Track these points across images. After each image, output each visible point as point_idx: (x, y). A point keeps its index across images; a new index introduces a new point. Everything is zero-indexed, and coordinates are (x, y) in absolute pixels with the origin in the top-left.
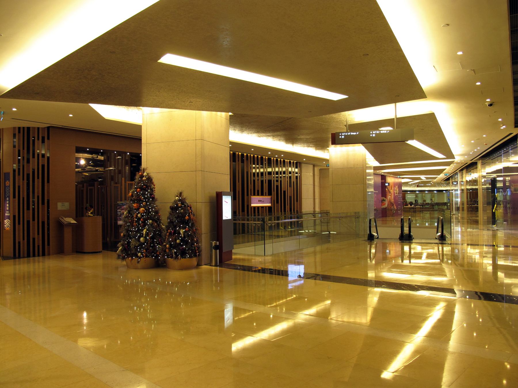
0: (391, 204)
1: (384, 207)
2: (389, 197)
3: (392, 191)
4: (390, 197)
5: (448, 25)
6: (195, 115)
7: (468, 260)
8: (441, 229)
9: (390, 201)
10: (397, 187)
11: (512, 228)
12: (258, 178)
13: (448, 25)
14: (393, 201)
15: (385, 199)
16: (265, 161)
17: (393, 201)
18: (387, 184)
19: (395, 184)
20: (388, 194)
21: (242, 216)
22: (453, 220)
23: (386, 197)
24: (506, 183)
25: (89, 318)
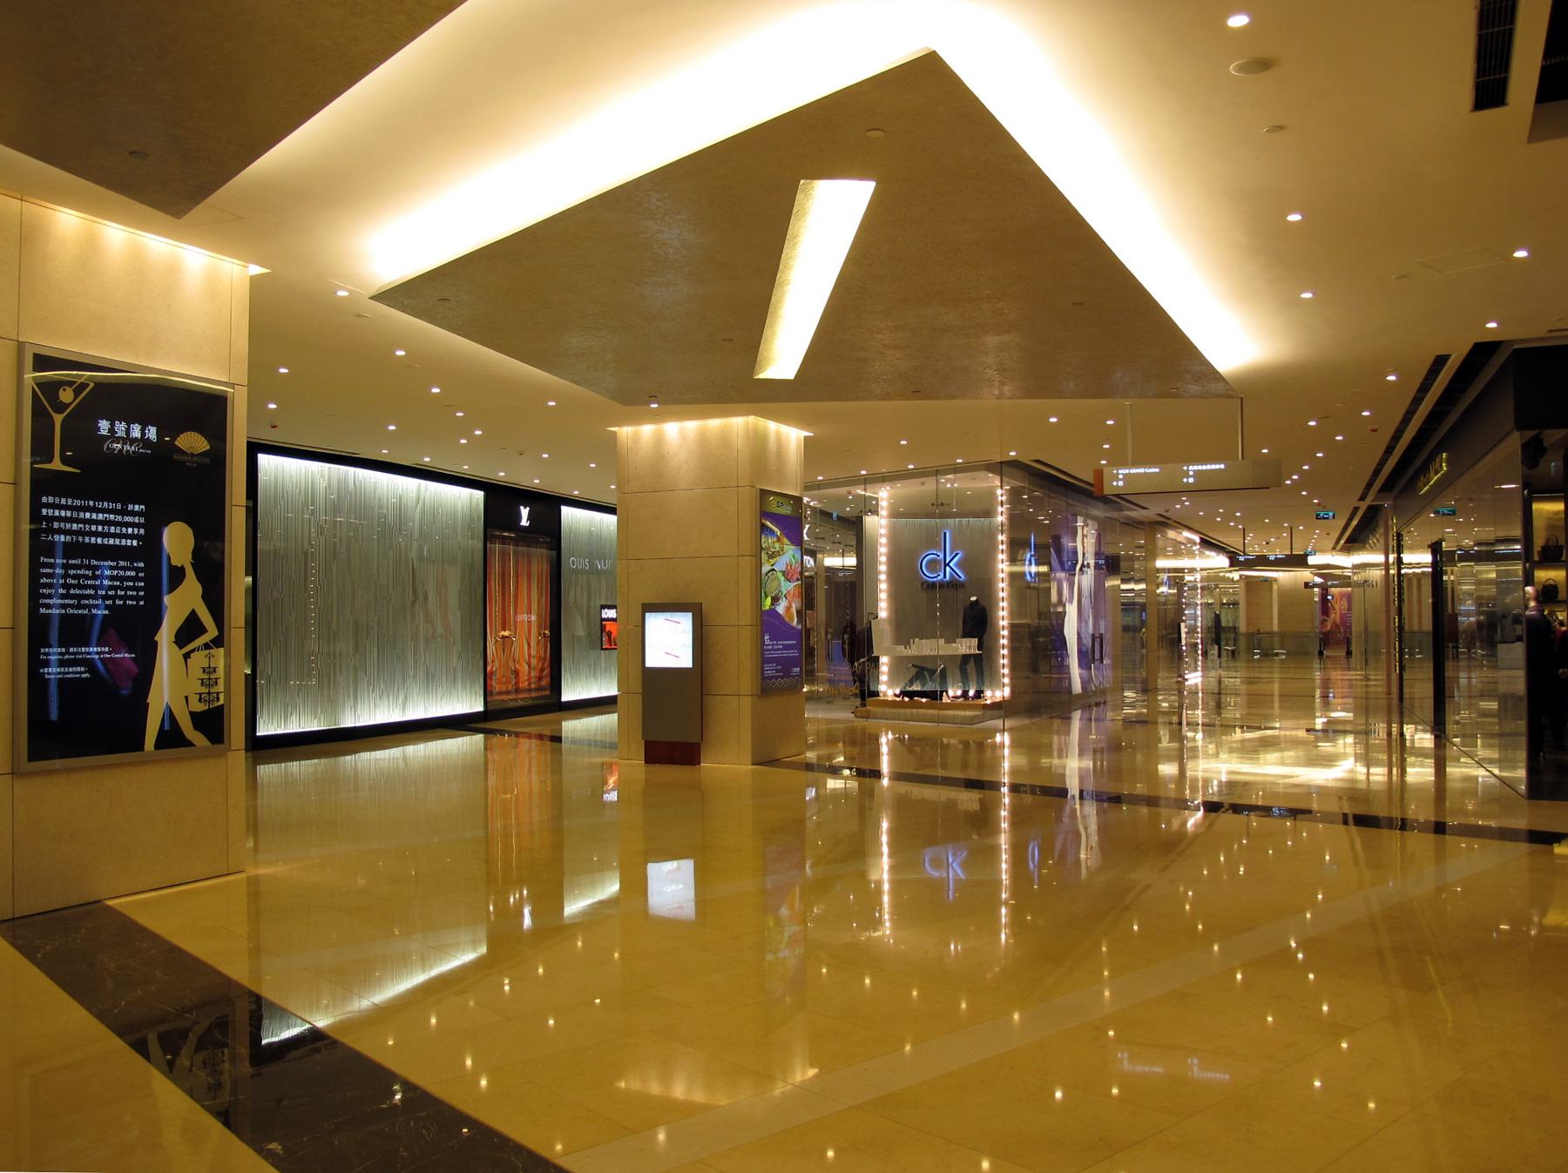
0: (1336, 625)
1: (1325, 630)
2: (1332, 616)
3: (1337, 607)
4: (1335, 616)
5: (1280, 128)
6: (19, 218)
7: (533, 686)
8: (244, 634)
9: (1334, 623)
10: (1345, 600)
11: (1102, 595)
12: (544, 738)
13: (1280, 128)
14: (1338, 621)
15: (1326, 618)
16: (498, 624)
17: (1338, 621)
18: (1329, 597)
19: (1342, 596)
20: (1331, 611)
21: (1202, 778)
22: (1333, 615)
23: (1328, 616)
24: (1430, 570)
25: (1504, 925)
